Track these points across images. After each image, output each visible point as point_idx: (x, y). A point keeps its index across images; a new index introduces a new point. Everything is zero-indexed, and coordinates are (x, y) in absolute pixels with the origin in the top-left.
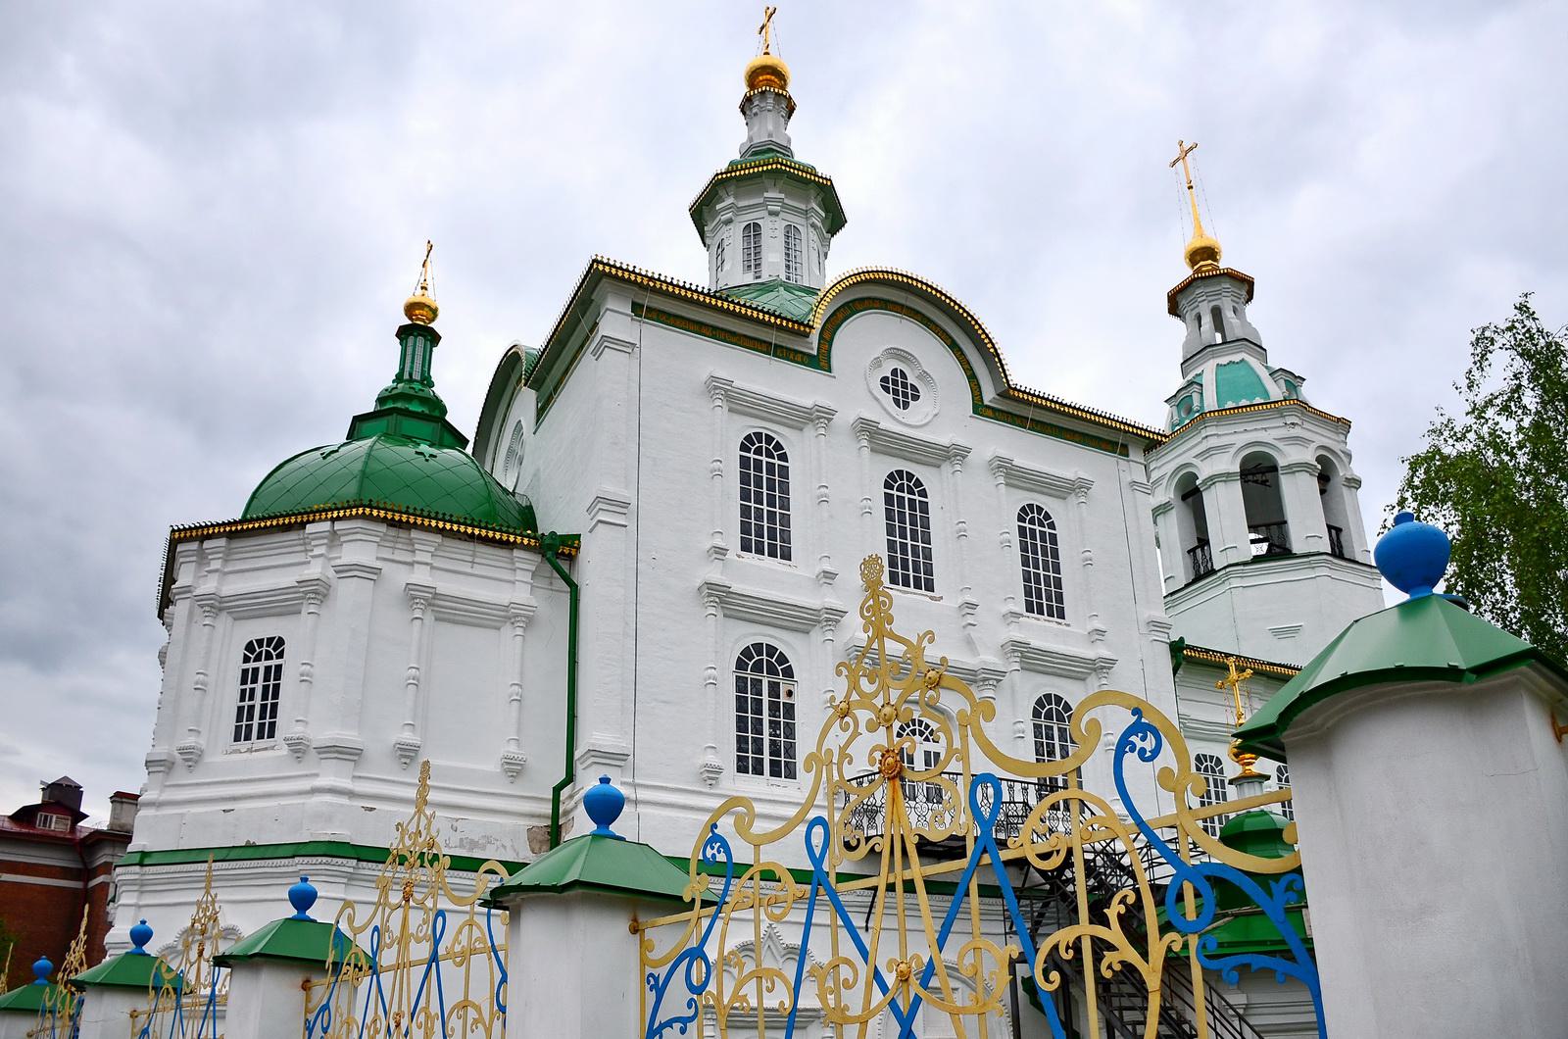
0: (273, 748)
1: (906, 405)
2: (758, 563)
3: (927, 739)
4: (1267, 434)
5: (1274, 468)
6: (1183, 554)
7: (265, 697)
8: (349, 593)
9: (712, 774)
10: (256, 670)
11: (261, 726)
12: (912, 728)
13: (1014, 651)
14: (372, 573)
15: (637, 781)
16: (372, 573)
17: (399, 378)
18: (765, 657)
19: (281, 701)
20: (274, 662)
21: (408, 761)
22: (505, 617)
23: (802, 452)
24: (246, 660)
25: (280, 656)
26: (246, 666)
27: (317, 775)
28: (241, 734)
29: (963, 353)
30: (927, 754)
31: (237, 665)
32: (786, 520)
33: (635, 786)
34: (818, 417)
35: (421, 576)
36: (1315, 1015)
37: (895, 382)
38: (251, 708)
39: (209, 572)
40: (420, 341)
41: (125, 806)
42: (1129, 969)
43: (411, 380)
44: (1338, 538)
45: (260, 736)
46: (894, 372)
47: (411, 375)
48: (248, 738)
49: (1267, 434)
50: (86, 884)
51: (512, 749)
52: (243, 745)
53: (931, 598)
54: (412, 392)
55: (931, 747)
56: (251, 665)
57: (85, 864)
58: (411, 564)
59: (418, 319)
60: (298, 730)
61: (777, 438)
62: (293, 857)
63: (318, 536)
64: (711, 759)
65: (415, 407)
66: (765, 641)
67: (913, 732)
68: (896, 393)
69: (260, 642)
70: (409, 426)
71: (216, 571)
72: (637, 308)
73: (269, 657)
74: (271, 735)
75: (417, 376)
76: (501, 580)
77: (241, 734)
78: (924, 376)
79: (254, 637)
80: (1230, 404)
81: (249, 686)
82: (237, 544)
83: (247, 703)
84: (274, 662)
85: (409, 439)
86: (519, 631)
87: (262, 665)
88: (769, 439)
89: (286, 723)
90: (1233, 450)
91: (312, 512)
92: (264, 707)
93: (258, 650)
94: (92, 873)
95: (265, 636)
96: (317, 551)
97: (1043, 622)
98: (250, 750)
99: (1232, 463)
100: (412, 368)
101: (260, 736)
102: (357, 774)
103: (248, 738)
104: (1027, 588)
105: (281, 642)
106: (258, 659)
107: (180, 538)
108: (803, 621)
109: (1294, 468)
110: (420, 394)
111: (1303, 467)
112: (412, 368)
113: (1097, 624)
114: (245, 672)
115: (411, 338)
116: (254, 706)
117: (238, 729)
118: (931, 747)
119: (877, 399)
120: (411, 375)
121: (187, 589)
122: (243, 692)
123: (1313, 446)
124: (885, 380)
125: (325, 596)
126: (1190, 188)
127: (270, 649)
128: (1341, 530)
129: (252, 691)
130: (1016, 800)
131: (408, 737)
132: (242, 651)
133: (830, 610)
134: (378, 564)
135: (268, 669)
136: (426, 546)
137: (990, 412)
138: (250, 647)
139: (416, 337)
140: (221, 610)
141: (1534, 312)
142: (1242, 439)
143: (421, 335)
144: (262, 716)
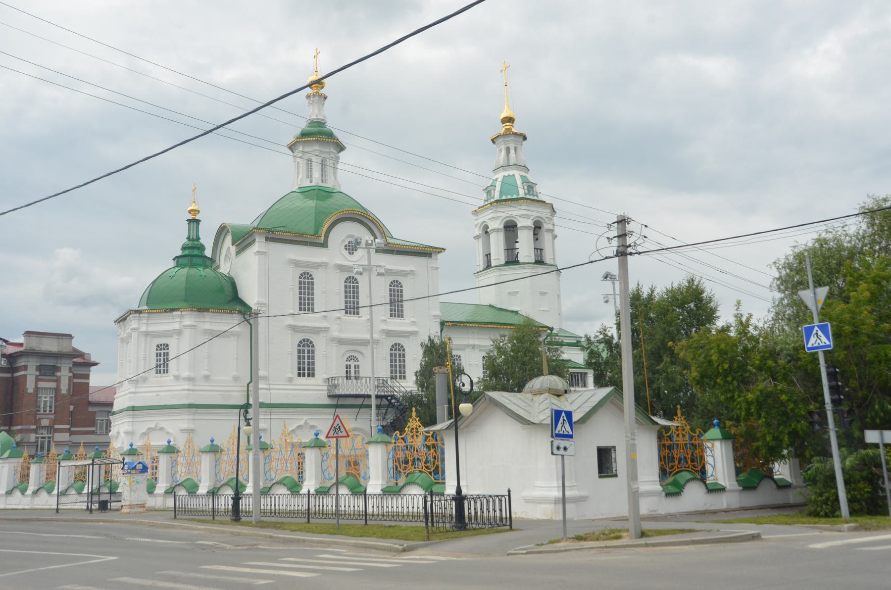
0: (168, 376)
1: (353, 253)
4: (516, 213)
5: (516, 226)
9: (290, 380)
11: (164, 370)
15: (268, 391)
17: (188, 238)
20: (166, 351)
23: (319, 278)
24: (157, 350)
25: (168, 349)
29: (373, 231)
30: (355, 366)
31: (154, 352)
32: (313, 299)
33: (269, 384)
34: (324, 265)
37: (349, 246)
41: (31, 338)
44: (541, 253)
45: (164, 373)
46: (349, 242)
48: (160, 373)
49: (516, 213)
50: (13, 375)
51: (235, 373)
52: (159, 375)
53: (359, 317)
55: (357, 363)
56: (159, 352)
57: (11, 366)
61: (310, 273)
63: (177, 315)
64: (290, 375)
66: (306, 338)
69: (161, 345)
72: (267, 239)
73: (164, 349)
74: (167, 372)
79: (159, 343)
80: (504, 198)
82: (151, 315)
86: (236, 338)
87: (162, 352)
88: (308, 273)
90: (501, 219)
94: (17, 369)
97: (397, 320)
98: (161, 377)
99: (500, 224)
103: (160, 373)
106: (161, 350)
108: (317, 331)
109: (523, 228)
111: (528, 228)
113: (413, 319)
114: (157, 354)
118: (357, 363)
119: (343, 255)
122: (157, 360)
124: (346, 246)
126: (506, 85)
130: (559, 268)
131: (206, 373)
133: (325, 328)
134: (195, 324)
135: (164, 353)
138: (158, 346)
140: (148, 335)
141: (518, 242)
142: (504, 215)
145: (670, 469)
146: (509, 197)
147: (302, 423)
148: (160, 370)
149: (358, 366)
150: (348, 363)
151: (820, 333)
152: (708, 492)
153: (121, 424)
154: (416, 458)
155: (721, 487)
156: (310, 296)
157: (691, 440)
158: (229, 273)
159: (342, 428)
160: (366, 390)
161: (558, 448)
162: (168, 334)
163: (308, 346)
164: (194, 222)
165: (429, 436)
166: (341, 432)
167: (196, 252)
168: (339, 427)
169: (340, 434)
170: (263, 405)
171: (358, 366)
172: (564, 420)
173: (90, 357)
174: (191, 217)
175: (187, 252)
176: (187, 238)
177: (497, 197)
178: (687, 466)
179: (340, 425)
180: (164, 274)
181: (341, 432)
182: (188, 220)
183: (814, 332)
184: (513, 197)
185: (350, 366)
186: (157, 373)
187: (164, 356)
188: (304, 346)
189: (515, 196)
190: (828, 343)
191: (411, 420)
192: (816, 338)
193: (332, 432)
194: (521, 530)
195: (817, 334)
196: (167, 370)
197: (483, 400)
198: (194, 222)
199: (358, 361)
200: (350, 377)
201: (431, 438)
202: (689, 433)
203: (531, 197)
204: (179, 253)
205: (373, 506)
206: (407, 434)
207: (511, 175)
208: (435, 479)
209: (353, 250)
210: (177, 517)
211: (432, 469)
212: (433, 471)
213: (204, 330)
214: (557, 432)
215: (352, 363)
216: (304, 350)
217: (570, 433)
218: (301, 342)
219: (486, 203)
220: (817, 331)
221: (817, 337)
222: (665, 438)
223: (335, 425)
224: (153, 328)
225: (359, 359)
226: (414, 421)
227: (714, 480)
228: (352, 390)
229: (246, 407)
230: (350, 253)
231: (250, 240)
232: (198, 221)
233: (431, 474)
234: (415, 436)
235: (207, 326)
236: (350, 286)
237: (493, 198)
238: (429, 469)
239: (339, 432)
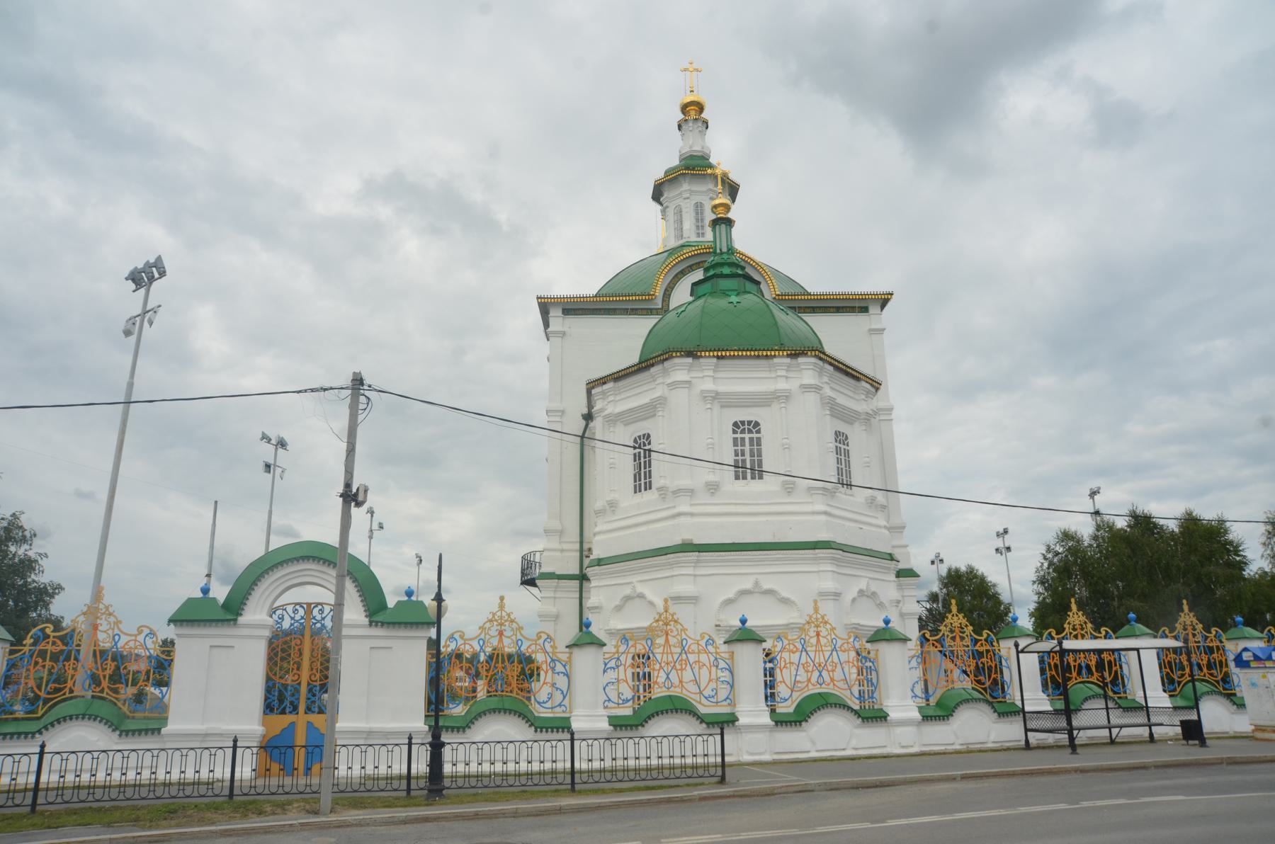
7: (752, 455)
8: (679, 398)
10: (743, 439)
13: (829, 403)
14: (688, 384)
16: (688, 384)
21: (790, 490)
22: (773, 398)
24: (735, 432)
27: (674, 507)
28: (637, 489)
35: (709, 385)
36: (1180, 728)
39: (609, 402)
40: (723, 226)
42: (991, 666)
43: (722, 253)
47: (721, 250)
48: (640, 491)
54: (723, 261)
58: (703, 377)
59: (719, 213)
60: (662, 482)
62: (814, 549)
65: (726, 270)
69: (743, 423)
70: (725, 284)
71: (611, 401)
74: (650, 488)
75: (725, 250)
76: (640, 393)
77: (637, 489)
79: (738, 419)
82: (722, 362)
85: (725, 293)
89: (657, 481)
91: (651, 359)
93: (639, 442)
95: (746, 419)
100: (721, 245)
101: (646, 489)
102: (692, 503)
103: (640, 491)
105: (649, 436)
106: (743, 432)
107: (592, 385)
110: (728, 261)
112: (721, 245)
114: (735, 440)
115: (718, 226)
116: (745, 460)
117: (635, 486)
120: (721, 250)
121: (602, 410)
123: (28, 645)
125: (665, 404)
127: (645, 440)
132: (731, 427)
135: (751, 439)
136: (708, 363)
138: (735, 424)
139: (720, 225)
140: (616, 421)
143: (722, 223)
145: (49, 693)
147: (748, 585)
152: (1000, 716)
154: (1083, 664)
155: (1138, 705)
157: (975, 645)
165: (981, 640)
173: (585, 414)
178: (509, 690)
186: (737, 478)
191: (1182, 615)
194: (812, 791)
201: (983, 642)
202: (971, 636)
205: (589, 758)
206: (1179, 632)
208: (1224, 689)
210: (577, 787)
211: (988, 684)
212: (1110, 681)
213: (702, 392)
222: (931, 642)
224: (727, 386)
226: (1076, 616)
227: (563, 712)
233: (1219, 685)
234: (958, 639)
238: (983, 684)
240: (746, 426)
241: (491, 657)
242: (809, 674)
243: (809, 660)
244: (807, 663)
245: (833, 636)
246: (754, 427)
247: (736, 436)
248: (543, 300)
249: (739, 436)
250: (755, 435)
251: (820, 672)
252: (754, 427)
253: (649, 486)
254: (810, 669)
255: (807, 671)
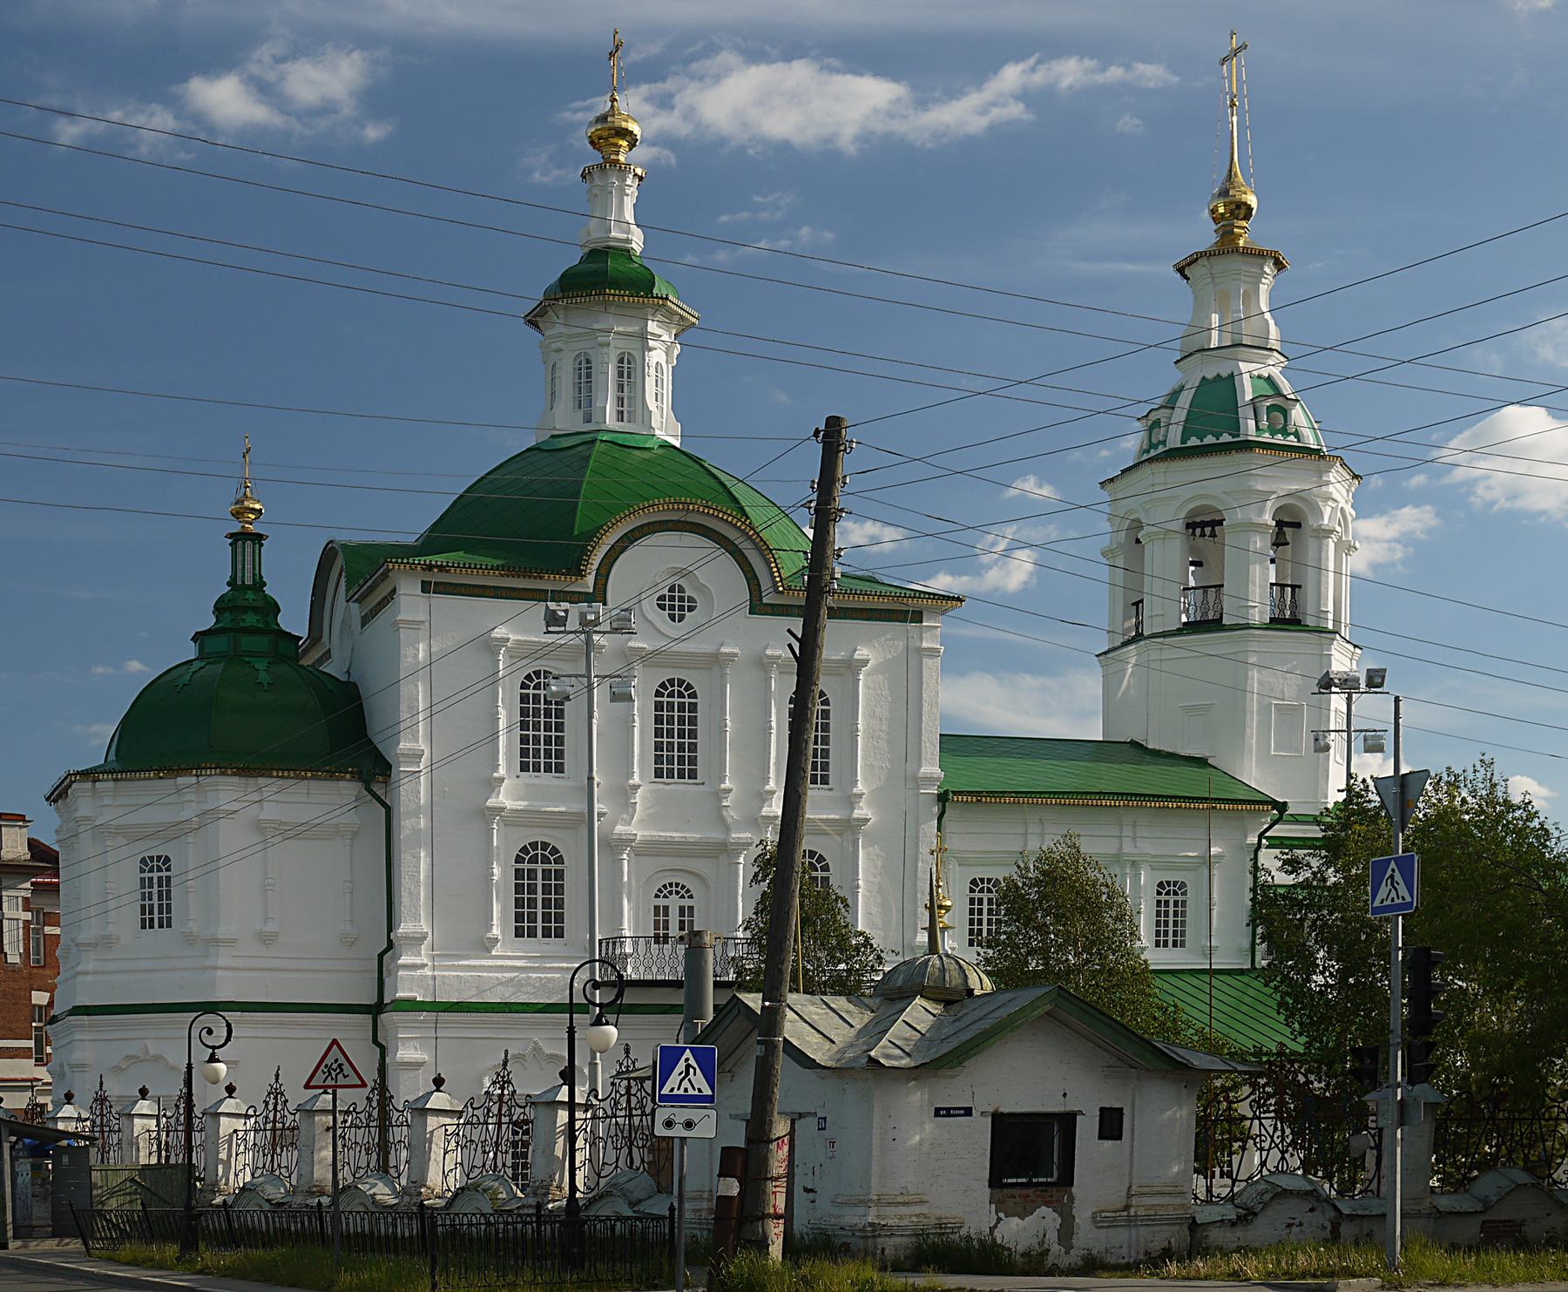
2: (536, 781)
3: (683, 897)
6: (1125, 606)
7: (160, 898)
10: (151, 879)
12: (679, 889)
18: (540, 852)
19: (173, 914)
26: (143, 875)
28: (146, 924)
30: (682, 909)
37: (672, 598)
38: (152, 906)
45: (161, 926)
46: (672, 589)
48: (152, 927)
56: (147, 875)
67: (671, 893)
68: (681, 599)
73: (160, 869)
77: (146, 924)
78: (702, 588)
80: (1193, 441)
81: (147, 890)
83: (147, 902)
84: (164, 874)
87: (155, 875)
92: (160, 906)
95: (1172, 880)
96: (188, 797)
101: (161, 926)
104: (560, 920)
117: (143, 921)
118: (687, 902)
124: (662, 598)
128: (1300, 587)
129: (150, 893)
135: (160, 878)
137: (769, 609)
144: (160, 912)
146: (1210, 440)
148: (152, 920)
149: (691, 908)
150: (661, 902)
151: (1398, 877)
153: (90, 1040)
156: (553, 734)
158: (348, 672)
159: (346, 1067)
160: (661, 969)
161: (669, 1124)
162: (177, 831)
163: (546, 860)
164: (246, 540)
166: (345, 1077)
167: (251, 619)
168: (340, 1066)
169: (341, 1081)
170: (412, 1006)
171: (691, 908)
172: (688, 1067)
174: (236, 527)
175: (226, 622)
176: (229, 584)
177: (1174, 441)
179: (342, 1060)
180: (163, 679)
181: (345, 1077)
182: (231, 536)
183: (1389, 873)
184: (1222, 440)
185: (666, 908)
187: (160, 885)
188: (533, 860)
189: (1226, 438)
190: (1408, 899)
192: (1389, 886)
193: (320, 1077)
195: (1392, 877)
196: (169, 919)
197: (735, 1012)
198: (246, 540)
199: (691, 897)
200: (666, 937)
203: (1279, 439)
204: (209, 622)
207: (1224, 374)
209: (681, 608)
214: (665, 1091)
215: (674, 903)
216: (535, 871)
217: (707, 1091)
218: (524, 850)
219: (1145, 457)
220: (1393, 870)
221: (1392, 884)
223: (328, 1061)
225: (693, 892)
228: (661, 969)
229: (376, 1009)
230: (672, 618)
231: (383, 591)
232: (258, 538)
235: (270, 812)
236: (671, 706)
237: (1164, 443)
239: (340, 1076)
240: (676, 688)
241: (243, 1189)
242: (1264, 1153)
243: (1263, 1132)
244: (1261, 1135)
245: (644, 1094)
246: (164, 864)
247: (143, 875)
248: (617, 292)
249: (147, 875)
250: (164, 874)
251: (1283, 1152)
252: (164, 864)
253: (166, 923)
254: (1266, 1145)
255: (1262, 1149)
